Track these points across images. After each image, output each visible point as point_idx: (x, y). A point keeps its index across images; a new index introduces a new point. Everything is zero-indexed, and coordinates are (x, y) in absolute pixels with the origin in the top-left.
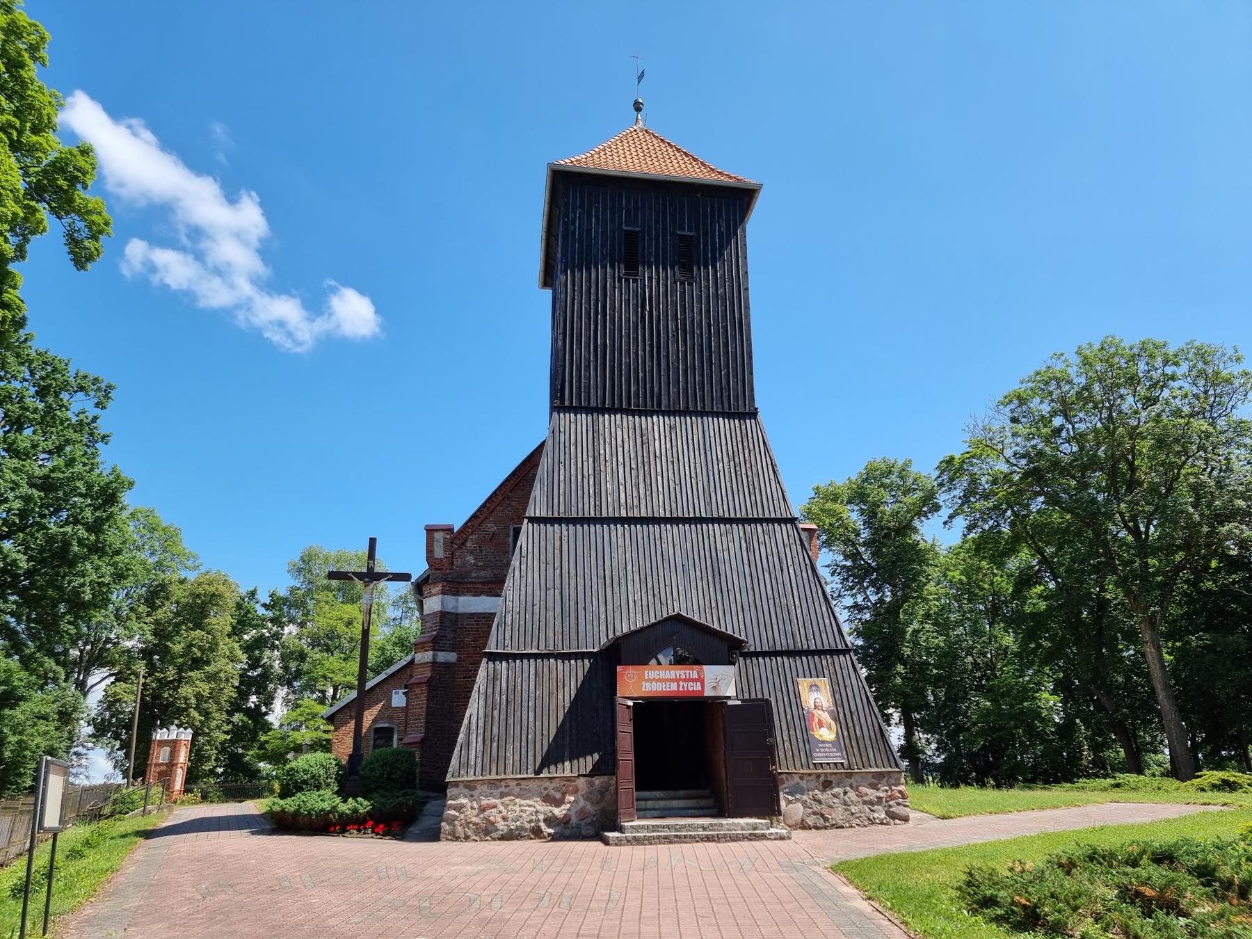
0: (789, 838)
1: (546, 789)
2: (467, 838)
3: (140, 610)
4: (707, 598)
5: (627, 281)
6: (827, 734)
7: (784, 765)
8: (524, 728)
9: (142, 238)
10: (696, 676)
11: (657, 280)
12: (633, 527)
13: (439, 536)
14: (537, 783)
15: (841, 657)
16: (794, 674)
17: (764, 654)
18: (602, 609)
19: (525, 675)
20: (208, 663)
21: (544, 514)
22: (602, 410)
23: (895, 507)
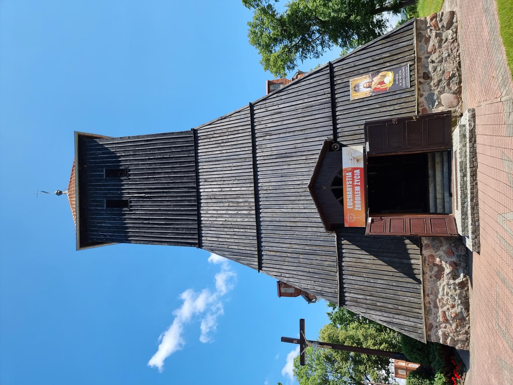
0: (474, 110)
1: (431, 277)
2: (467, 333)
3: (337, 367)
4: (300, 162)
5: (131, 206)
6: (389, 78)
7: (412, 111)
8: (389, 287)
9: (199, 337)
10: (350, 174)
11: (129, 190)
12: (261, 207)
13: (283, 290)
14: (427, 283)
15: (335, 70)
16: (347, 103)
17: (335, 124)
18: (310, 229)
19: (353, 282)
20: (359, 339)
21: (257, 260)
22: (199, 221)
23: (270, 29)
